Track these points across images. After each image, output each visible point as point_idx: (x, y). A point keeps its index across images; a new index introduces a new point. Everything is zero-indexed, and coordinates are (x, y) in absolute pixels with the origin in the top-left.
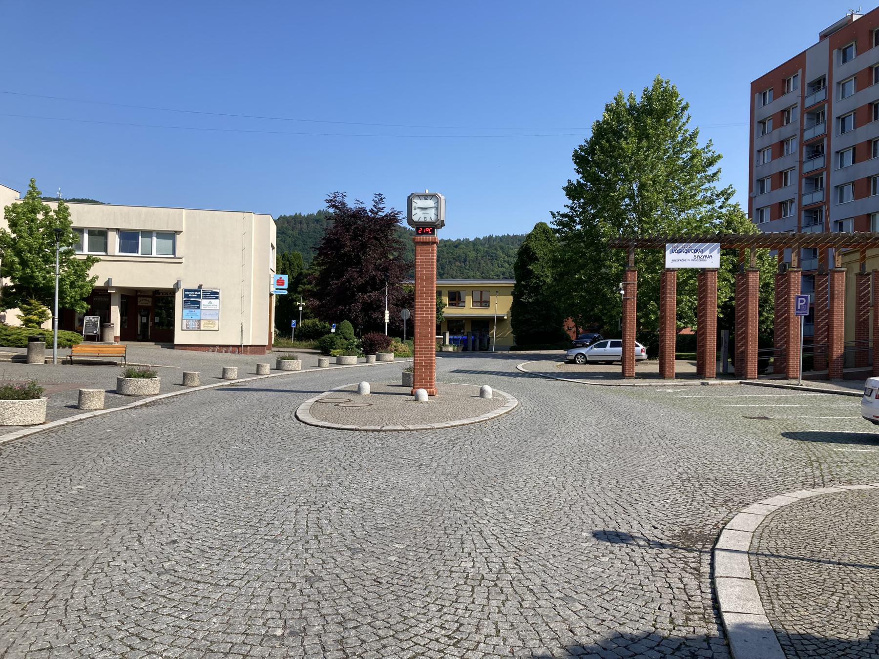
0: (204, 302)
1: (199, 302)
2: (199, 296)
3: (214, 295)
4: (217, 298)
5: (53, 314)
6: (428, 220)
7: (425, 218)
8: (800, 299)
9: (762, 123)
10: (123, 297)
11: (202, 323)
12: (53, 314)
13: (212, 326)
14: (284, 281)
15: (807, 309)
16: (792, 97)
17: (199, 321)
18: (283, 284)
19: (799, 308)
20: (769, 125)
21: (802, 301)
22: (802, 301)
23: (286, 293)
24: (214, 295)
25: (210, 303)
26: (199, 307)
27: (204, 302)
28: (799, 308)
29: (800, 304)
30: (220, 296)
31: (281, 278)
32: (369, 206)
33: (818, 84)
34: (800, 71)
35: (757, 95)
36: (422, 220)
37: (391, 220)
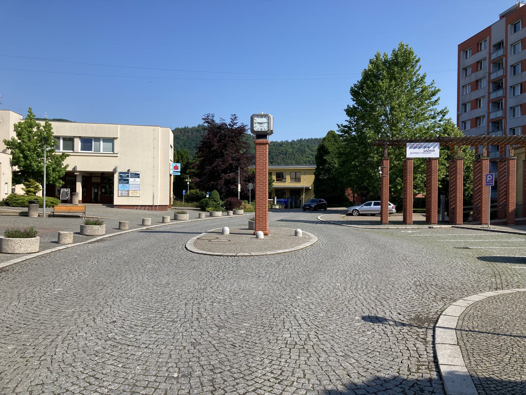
0: (131, 180)
1: (128, 180)
2: (128, 176)
3: (137, 175)
4: (139, 177)
6: (263, 130)
7: (261, 129)
8: (488, 176)
10: (83, 177)
11: (130, 192)
13: (136, 194)
14: (178, 167)
15: (492, 182)
16: (483, 54)
17: (128, 191)
18: (178, 169)
19: (488, 181)
20: (469, 71)
21: (489, 177)
22: (489, 177)
24: (137, 175)
26: (128, 183)
27: (131, 180)
28: (488, 181)
29: (488, 179)
30: (141, 176)
31: (176, 165)
32: (228, 122)
33: (499, 46)
36: (259, 130)
37: (241, 130)
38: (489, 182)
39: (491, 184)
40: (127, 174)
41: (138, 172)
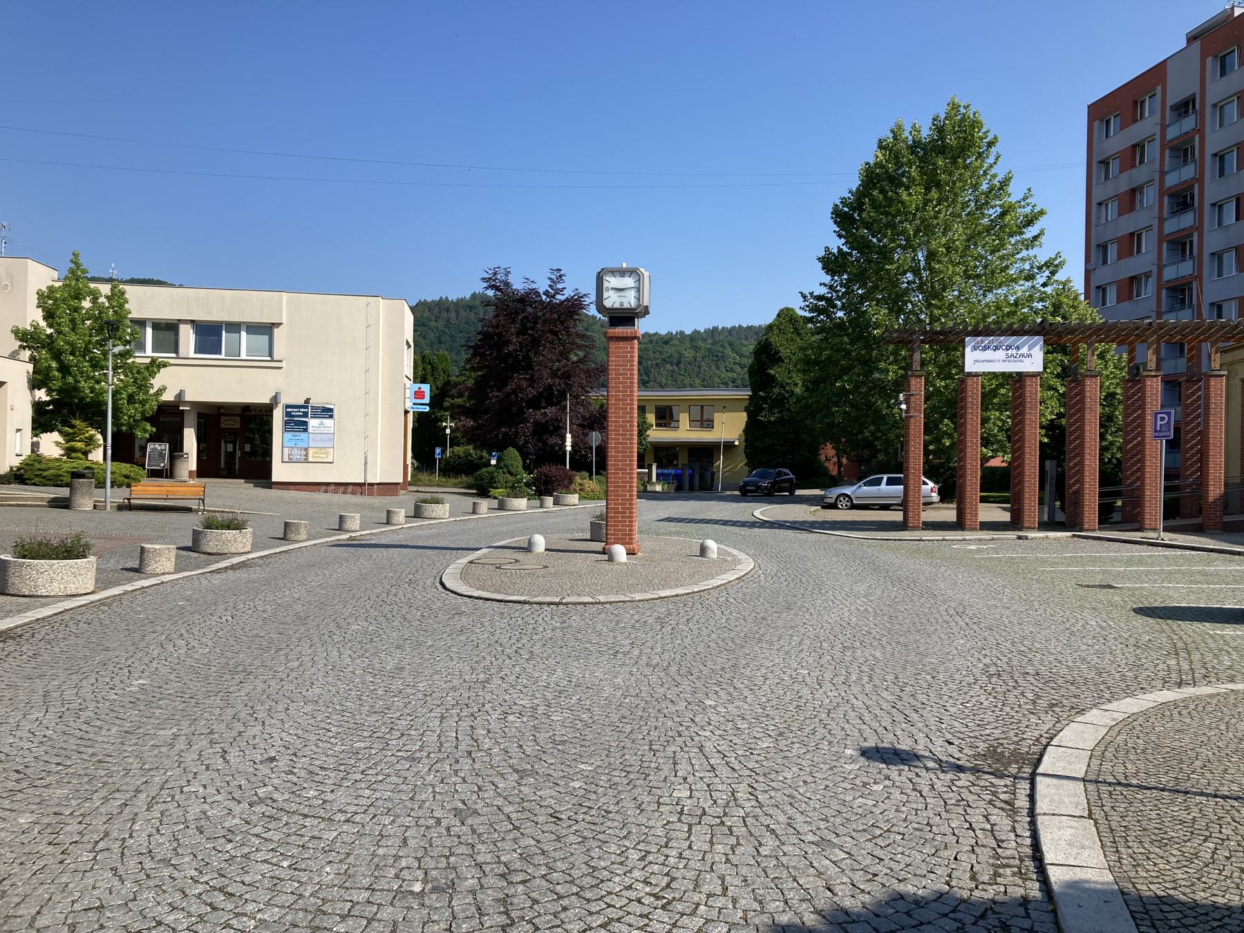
0: (313, 423)
1: (306, 423)
2: (306, 414)
3: (327, 412)
4: (331, 417)
5: (105, 440)
6: (626, 305)
7: (622, 303)
9: (1105, 163)
10: (200, 415)
11: (311, 452)
12: (105, 440)
13: (325, 456)
14: (424, 392)
15: (1169, 430)
16: (1148, 125)
17: (306, 449)
19: (1158, 429)
20: (1114, 167)
21: (1162, 419)
22: (1162, 419)
23: (427, 409)
24: (327, 412)
25: (322, 423)
26: (306, 430)
27: (313, 423)
28: (1158, 429)
29: (1159, 423)
30: (336, 413)
31: (420, 388)
32: (542, 286)
33: (1184, 107)
34: (1159, 89)
35: (1096, 124)
36: (617, 305)
37: (573, 307)
38: (1160, 431)
39: (1165, 434)
40: (302, 410)
41: (331, 404)
